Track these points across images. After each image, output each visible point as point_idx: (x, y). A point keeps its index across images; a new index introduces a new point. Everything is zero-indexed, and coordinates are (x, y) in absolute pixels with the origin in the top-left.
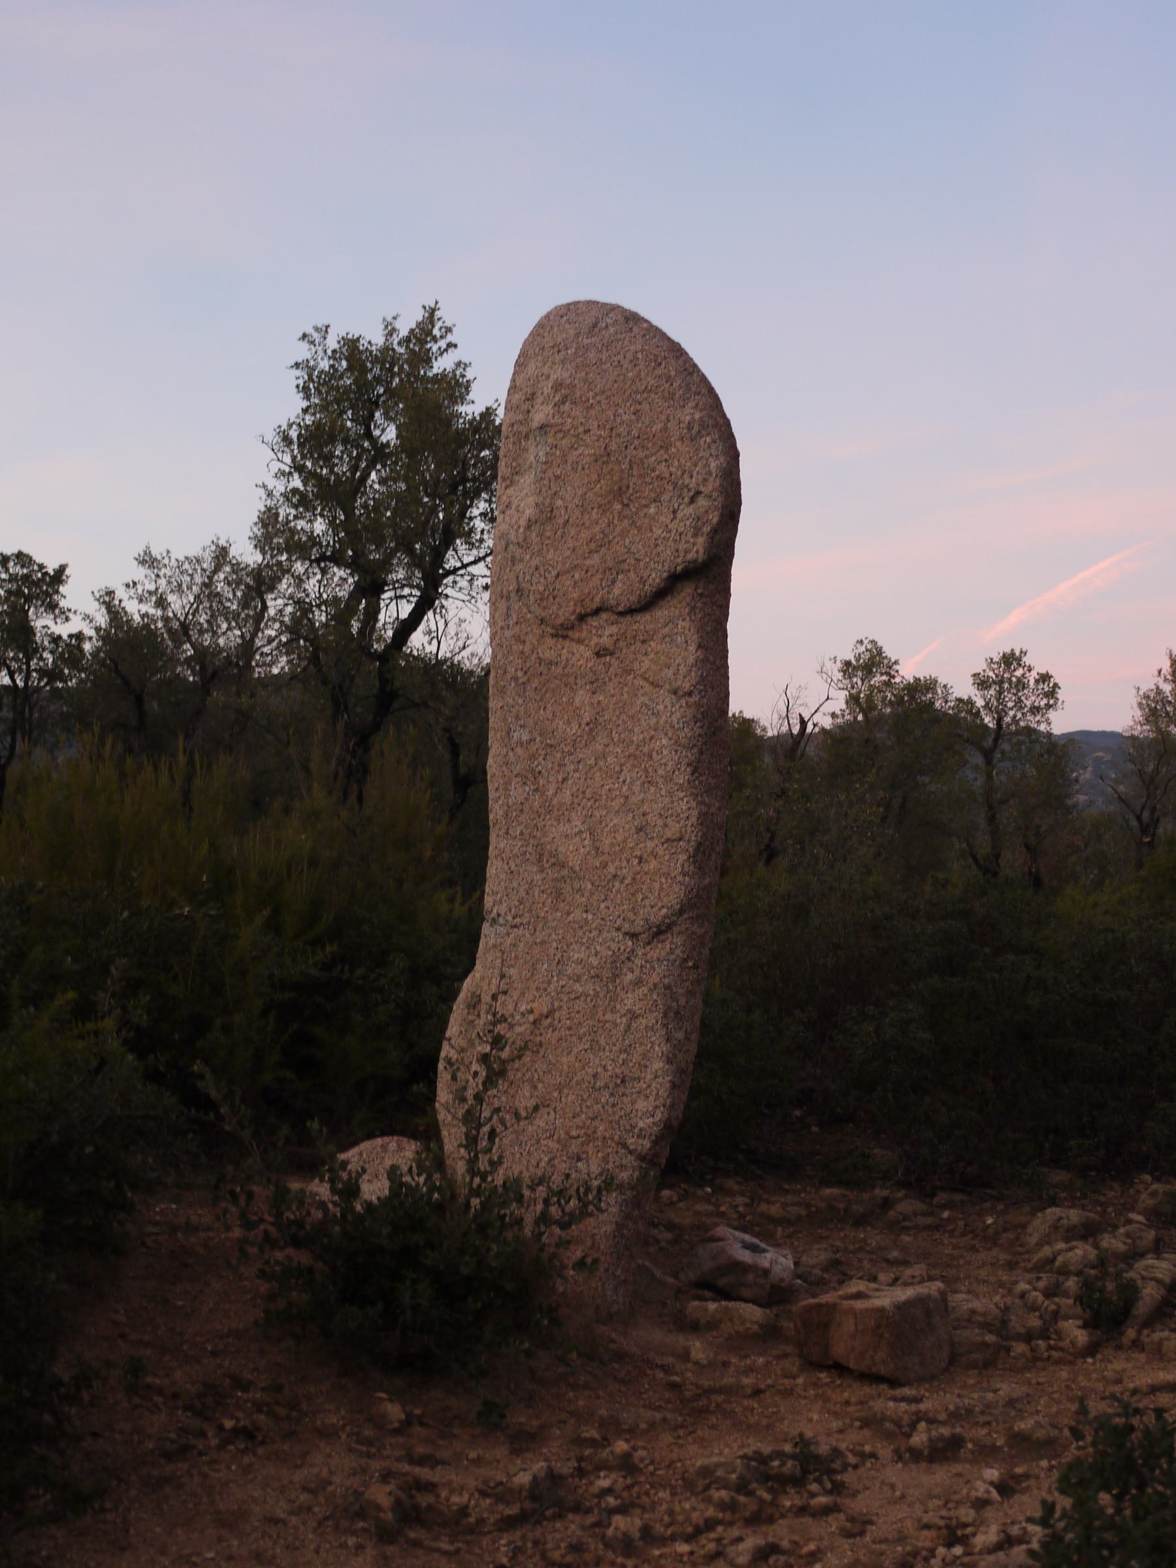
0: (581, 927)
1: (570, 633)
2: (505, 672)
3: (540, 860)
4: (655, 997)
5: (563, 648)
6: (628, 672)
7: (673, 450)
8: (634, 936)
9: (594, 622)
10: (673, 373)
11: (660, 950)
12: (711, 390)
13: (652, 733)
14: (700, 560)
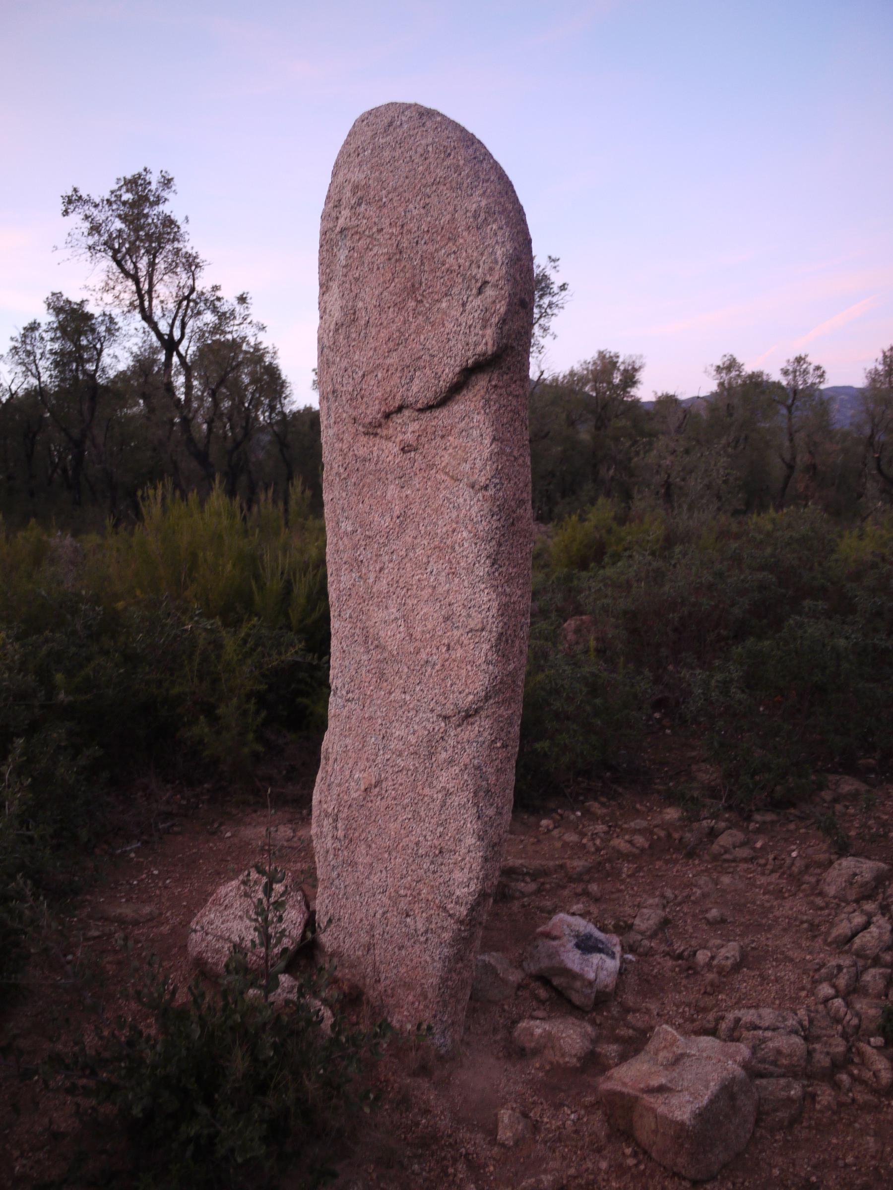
0: (401, 707)
1: (379, 431)
2: (331, 468)
3: (366, 642)
4: (466, 777)
5: (374, 445)
6: (431, 466)
7: (461, 241)
8: (446, 718)
9: (398, 419)
10: (462, 162)
11: (469, 732)
12: (502, 177)
13: (454, 526)
14: (490, 353)
